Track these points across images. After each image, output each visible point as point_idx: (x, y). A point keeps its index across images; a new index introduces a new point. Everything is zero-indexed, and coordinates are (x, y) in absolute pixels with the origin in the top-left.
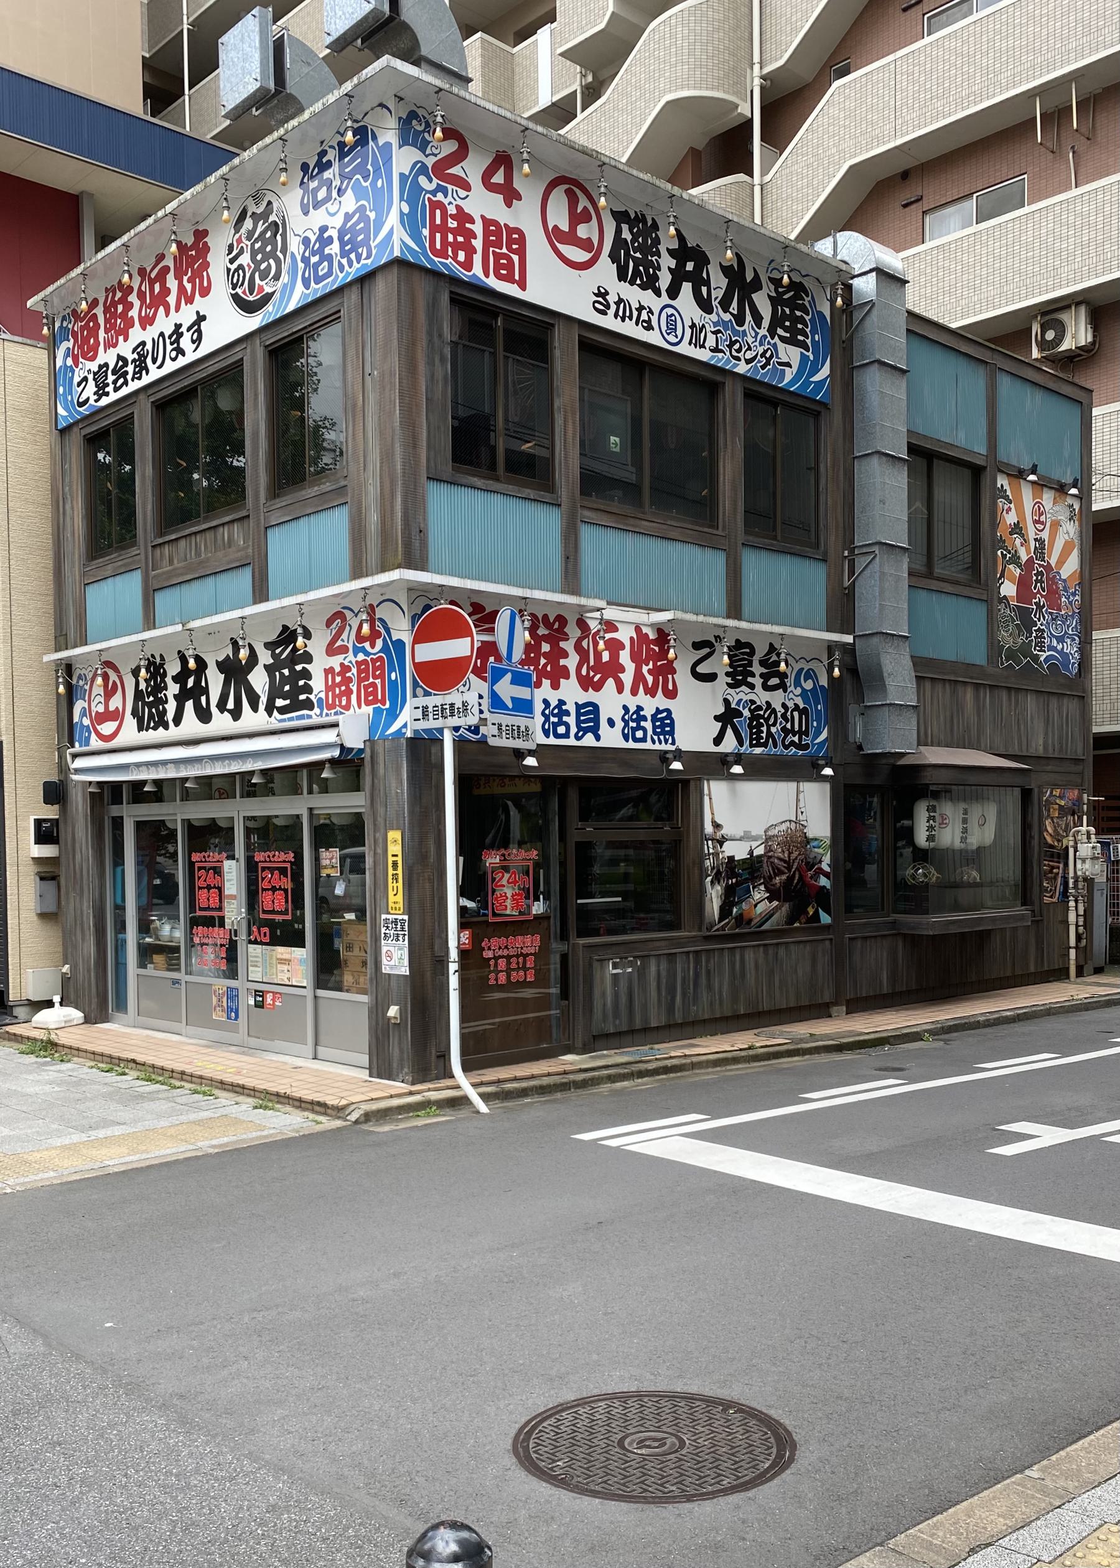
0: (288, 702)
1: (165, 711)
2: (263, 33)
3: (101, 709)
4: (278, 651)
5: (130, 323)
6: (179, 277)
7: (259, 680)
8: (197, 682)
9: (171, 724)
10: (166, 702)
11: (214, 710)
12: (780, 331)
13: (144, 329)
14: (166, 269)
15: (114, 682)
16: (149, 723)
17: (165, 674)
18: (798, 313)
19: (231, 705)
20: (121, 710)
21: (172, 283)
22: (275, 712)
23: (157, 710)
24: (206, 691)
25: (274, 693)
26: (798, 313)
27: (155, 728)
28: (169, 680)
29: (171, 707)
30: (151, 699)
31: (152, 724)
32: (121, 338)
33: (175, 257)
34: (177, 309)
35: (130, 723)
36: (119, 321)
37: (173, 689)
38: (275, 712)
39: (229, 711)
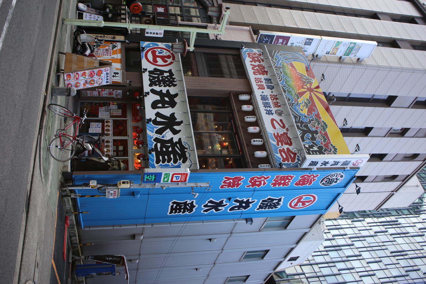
0: (159, 150)
1: (156, 85)
2: (326, 214)
3: (157, 54)
4: (178, 145)
6: (259, 66)
7: (168, 135)
8: (167, 102)
9: (151, 88)
10: (160, 86)
12: (175, 205)
15: (167, 61)
17: (170, 86)
18: (182, 210)
19: (159, 119)
21: (257, 63)
22: (155, 143)
23: (156, 81)
24: (163, 107)
25: (163, 142)
26: (182, 210)
27: (150, 80)
28: (167, 88)
29: (157, 88)
30: (161, 79)
34: (251, 65)
37: (164, 90)
38: (155, 143)
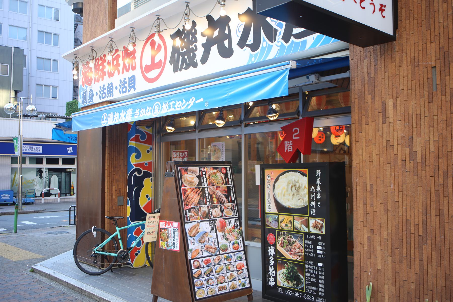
1: (195, 55)
5: (104, 74)
9: (199, 63)
10: (196, 49)
11: (235, 47)
13: (110, 78)
14: (119, 56)
16: (182, 65)
19: (250, 40)
20: (163, 61)
22: (292, 38)
27: (186, 68)
31: (184, 66)
32: (101, 79)
33: (122, 52)
34: (123, 73)
35: (169, 67)
36: (100, 72)
38: (292, 38)
39: (248, 46)
